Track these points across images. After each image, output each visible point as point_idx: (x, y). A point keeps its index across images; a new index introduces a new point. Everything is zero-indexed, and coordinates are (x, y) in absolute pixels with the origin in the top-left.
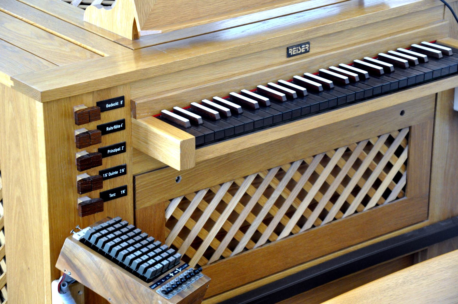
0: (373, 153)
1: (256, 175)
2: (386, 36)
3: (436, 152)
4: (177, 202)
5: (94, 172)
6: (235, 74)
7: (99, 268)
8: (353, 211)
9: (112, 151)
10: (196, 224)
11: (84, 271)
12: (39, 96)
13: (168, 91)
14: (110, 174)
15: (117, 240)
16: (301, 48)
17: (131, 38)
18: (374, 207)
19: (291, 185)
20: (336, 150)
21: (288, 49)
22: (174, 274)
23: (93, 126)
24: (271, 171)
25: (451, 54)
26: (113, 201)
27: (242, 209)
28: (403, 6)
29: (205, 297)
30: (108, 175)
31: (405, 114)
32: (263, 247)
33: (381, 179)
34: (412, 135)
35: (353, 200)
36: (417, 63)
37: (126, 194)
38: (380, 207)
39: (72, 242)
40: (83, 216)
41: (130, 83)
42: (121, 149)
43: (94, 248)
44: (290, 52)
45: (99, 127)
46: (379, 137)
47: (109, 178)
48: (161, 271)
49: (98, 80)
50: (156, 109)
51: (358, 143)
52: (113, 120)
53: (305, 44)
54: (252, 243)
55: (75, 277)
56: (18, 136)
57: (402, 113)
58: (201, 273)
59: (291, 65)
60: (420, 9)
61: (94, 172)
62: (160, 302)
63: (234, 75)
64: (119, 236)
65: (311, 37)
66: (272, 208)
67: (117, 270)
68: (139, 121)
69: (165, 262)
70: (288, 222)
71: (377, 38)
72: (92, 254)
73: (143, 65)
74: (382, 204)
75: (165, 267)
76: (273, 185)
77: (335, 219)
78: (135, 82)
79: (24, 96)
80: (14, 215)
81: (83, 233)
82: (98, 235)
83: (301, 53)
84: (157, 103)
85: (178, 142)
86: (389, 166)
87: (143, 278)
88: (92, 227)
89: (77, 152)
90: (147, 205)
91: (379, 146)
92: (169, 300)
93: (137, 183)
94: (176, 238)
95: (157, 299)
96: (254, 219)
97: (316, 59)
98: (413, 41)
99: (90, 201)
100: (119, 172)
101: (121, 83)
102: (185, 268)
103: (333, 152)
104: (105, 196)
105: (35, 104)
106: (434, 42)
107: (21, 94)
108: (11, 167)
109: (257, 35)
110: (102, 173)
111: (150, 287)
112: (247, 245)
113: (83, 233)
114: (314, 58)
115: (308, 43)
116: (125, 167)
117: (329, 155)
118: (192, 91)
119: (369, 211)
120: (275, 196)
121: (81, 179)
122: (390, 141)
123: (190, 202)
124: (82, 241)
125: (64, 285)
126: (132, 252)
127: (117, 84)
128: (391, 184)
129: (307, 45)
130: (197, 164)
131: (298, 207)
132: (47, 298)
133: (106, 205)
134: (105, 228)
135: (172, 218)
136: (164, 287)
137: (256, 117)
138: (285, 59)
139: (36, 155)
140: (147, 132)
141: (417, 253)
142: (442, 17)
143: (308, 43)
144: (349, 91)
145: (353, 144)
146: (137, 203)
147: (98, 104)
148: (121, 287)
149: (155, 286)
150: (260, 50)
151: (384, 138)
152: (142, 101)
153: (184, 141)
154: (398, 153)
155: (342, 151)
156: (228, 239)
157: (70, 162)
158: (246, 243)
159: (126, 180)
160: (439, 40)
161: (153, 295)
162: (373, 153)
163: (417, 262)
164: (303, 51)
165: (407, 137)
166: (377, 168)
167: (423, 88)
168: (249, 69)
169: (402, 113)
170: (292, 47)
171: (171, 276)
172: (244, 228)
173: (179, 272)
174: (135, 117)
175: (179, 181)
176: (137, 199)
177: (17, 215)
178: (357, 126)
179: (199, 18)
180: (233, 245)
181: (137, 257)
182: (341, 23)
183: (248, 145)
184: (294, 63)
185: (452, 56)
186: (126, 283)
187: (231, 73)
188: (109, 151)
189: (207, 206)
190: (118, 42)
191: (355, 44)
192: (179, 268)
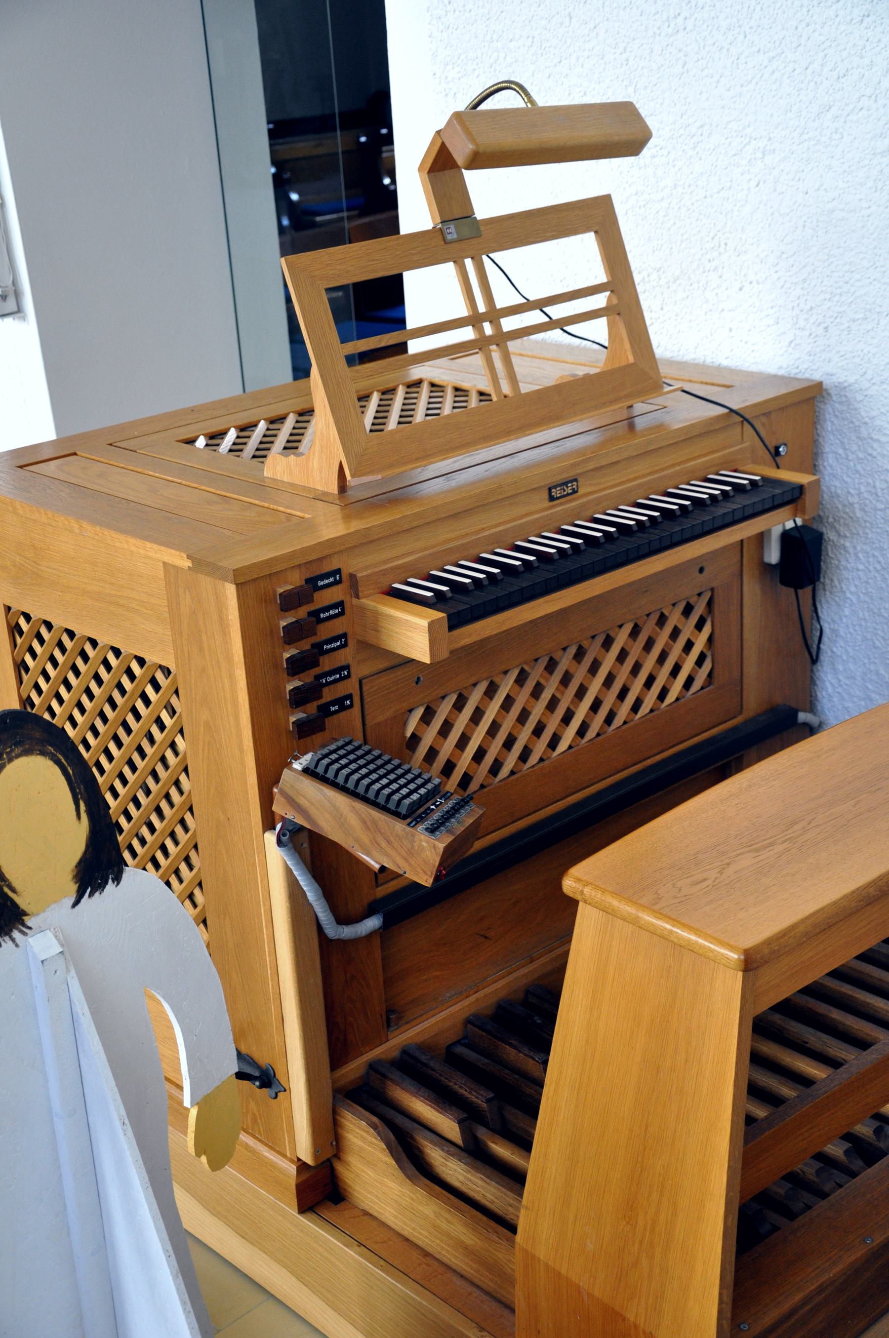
0: (668, 629)
1: (519, 668)
2: (673, 465)
3: (746, 621)
4: (419, 712)
5: (308, 677)
6: (483, 529)
7: (334, 806)
8: (648, 710)
9: (330, 646)
10: (445, 742)
11: (313, 812)
12: (231, 576)
13: (397, 558)
14: (329, 679)
15: (353, 766)
16: (567, 487)
17: (336, 492)
18: (673, 702)
19: (566, 680)
20: (620, 626)
21: (550, 490)
22: (437, 806)
23: (302, 612)
24: (539, 661)
25: (760, 484)
26: (335, 716)
27: (504, 718)
28: (692, 424)
29: (480, 835)
30: (326, 680)
31: (705, 572)
32: (536, 768)
33: (681, 664)
34: (716, 600)
35: (646, 695)
36: (720, 498)
37: (351, 706)
38: (682, 701)
39: (294, 774)
40: (300, 738)
41: (347, 549)
42: (341, 642)
43: (323, 779)
44: (553, 494)
45: (310, 614)
46: (674, 605)
47: (328, 684)
48: (419, 804)
49: (306, 548)
50: (384, 583)
51: (648, 615)
52: (327, 603)
53: (571, 481)
54: (521, 763)
55: (300, 821)
56: (201, 636)
57: (701, 570)
58: (471, 803)
59: (556, 512)
60: (712, 428)
61: (308, 677)
62: (424, 844)
63: (483, 529)
64: (355, 761)
65: (579, 471)
66: (543, 713)
67: (359, 806)
68: (364, 601)
69: (422, 791)
70: (565, 731)
71: (662, 470)
72: (322, 787)
73: (356, 525)
74: (683, 697)
75: (423, 798)
76: (543, 681)
77: (625, 723)
78: (354, 547)
79: (208, 579)
80: (201, 747)
81: (307, 759)
82: (325, 761)
83: (568, 494)
84: (384, 574)
85: (425, 623)
86: (689, 646)
87: (396, 814)
88: (316, 753)
89: (284, 651)
90: (381, 718)
91: (675, 618)
92: (437, 840)
93: (365, 689)
94: (421, 764)
95: (421, 840)
96: (521, 729)
97: (587, 502)
98: (709, 470)
99: (307, 717)
100: (340, 675)
101: (337, 550)
102: (449, 797)
103: (617, 629)
104: (324, 710)
105: (224, 587)
106: (735, 471)
107: (203, 576)
108: (193, 681)
109: (508, 473)
110: (318, 677)
111: (409, 824)
112: (514, 766)
113: (307, 759)
114: (584, 500)
115: (576, 480)
116: (347, 667)
117: (612, 634)
118: (430, 555)
119: (667, 708)
120: (546, 696)
121: (292, 688)
122: (688, 610)
123: (435, 712)
124: (306, 771)
125: (284, 835)
126: (377, 780)
127: (331, 551)
128: (693, 669)
129: (574, 483)
130: (452, 652)
131: (576, 709)
132: (258, 857)
133: (329, 721)
134: (334, 751)
135: (413, 735)
136: (428, 823)
137: (524, 582)
138: (547, 504)
139: (229, 659)
140: (376, 615)
141: (730, 762)
142: (739, 437)
143: (576, 480)
144: (641, 539)
145: (642, 617)
146: (367, 718)
147: (308, 581)
148: (368, 828)
149: (414, 823)
150: (514, 493)
151: (681, 607)
152: (365, 573)
153: (432, 621)
154: (699, 626)
155: (628, 628)
156: (489, 760)
157: (276, 665)
158: (513, 764)
159: (350, 687)
160: (741, 468)
161: (413, 836)
162: (668, 629)
163: (730, 775)
164: (570, 491)
165: (710, 604)
166: (674, 648)
167: (732, 531)
168: (501, 521)
169: (701, 570)
170: (555, 487)
171: (433, 809)
172: (509, 744)
173: (441, 803)
174: (358, 597)
175: (420, 683)
176: (366, 713)
177: (206, 747)
178: (646, 592)
179: (427, 456)
180: (495, 769)
181: (384, 787)
182: (615, 450)
183: (515, 623)
184: (560, 508)
185: (762, 486)
186: (374, 821)
187: (478, 527)
188: (325, 647)
189: (458, 716)
190: (321, 497)
191: (635, 479)
192: (441, 799)
